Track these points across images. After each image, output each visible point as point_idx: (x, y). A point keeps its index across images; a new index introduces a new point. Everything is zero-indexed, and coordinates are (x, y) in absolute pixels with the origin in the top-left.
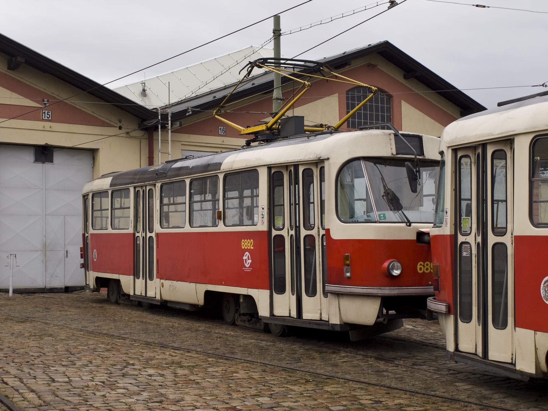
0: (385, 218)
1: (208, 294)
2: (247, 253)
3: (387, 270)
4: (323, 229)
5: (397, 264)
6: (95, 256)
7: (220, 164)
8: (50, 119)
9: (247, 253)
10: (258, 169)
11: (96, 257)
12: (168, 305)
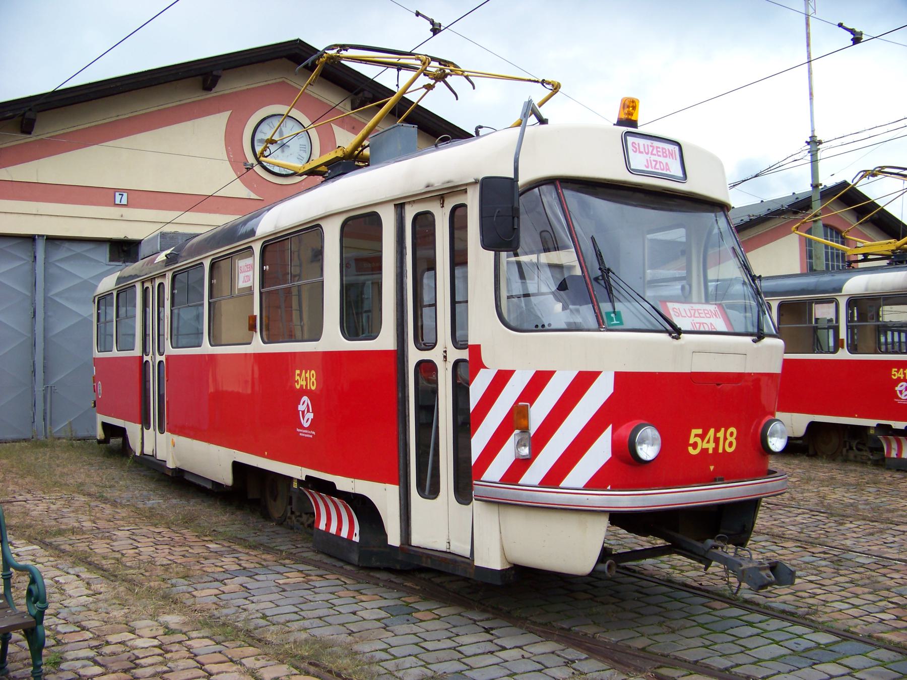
0: (621, 323)
1: (238, 468)
2: (305, 398)
5: (650, 432)
9: (305, 398)
10: (323, 223)
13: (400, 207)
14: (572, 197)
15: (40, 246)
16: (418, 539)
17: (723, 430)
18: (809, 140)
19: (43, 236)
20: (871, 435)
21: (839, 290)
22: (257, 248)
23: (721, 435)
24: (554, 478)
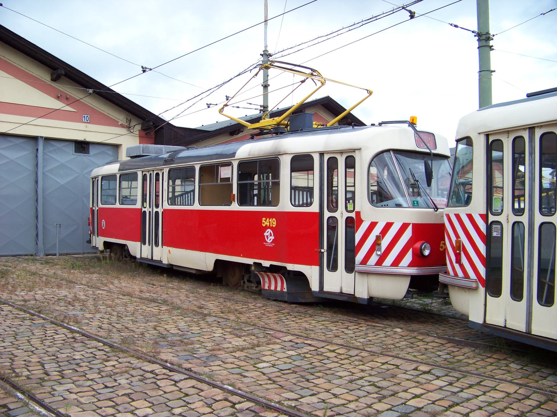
1: (218, 262)
3: (420, 254)
4: (98, 207)
6: (104, 225)
7: (235, 153)
8: (89, 121)
11: (105, 225)
12: (174, 268)
13: (322, 154)
14: (402, 158)
15: (41, 143)
16: (327, 288)
17: (271, 219)
18: (262, 53)
19: (42, 137)
20: (253, 271)
21: (233, 155)
22: (235, 164)
23: (271, 220)
24: (396, 263)
